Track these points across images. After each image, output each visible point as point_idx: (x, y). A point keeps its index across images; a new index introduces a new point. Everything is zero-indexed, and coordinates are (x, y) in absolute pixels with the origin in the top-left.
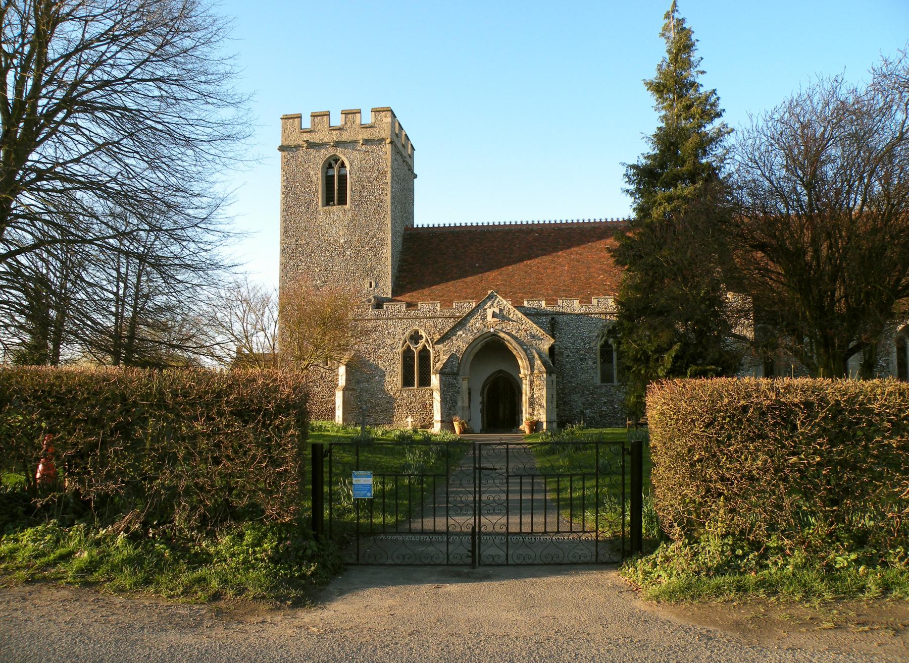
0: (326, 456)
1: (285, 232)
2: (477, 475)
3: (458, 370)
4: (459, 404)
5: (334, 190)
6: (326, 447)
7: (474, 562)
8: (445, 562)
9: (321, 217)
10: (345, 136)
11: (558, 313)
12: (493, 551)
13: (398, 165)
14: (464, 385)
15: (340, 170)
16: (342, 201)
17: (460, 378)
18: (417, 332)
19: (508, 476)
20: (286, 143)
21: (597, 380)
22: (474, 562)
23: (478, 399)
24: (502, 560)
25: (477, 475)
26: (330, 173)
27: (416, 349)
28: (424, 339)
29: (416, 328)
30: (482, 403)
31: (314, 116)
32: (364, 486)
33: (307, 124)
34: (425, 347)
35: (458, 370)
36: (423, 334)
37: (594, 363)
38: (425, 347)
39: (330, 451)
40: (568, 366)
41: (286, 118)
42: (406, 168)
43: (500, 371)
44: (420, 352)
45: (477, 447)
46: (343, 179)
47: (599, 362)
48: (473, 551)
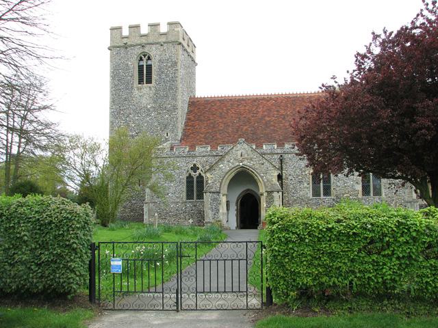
0: (96, 249)
1: (113, 102)
2: (179, 260)
3: (220, 190)
4: (221, 211)
5: (145, 75)
6: (97, 244)
7: (177, 308)
8: (245, 308)
9: (136, 92)
10: (151, 40)
11: (285, 153)
12: (189, 302)
13: (185, 58)
14: (224, 199)
15: (145, 63)
16: (149, 81)
17: (221, 195)
18: (195, 165)
19: (197, 260)
20: (113, 45)
21: (310, 195)
22: (177, 308)
23: (233, 208)
24: (194, 307)
25: (179, 260)
26: (141, 63)
27: (195, 175)
28: (200, 170)
29: (195, 162)
30: (237, 210)
31: (130, 27)
32: (117, 266)
33: (126, 32)
34: (200, 174)
35: (220, 190)
36: (200, 166)
37: (308, 184)
38: (200, 174)
39: (99, 247)
40: (291, 186)
41: (112, 29)
42: (190, 59)
43: (248, 190)
44: (197, 178)
45: (179, 244)
46: (149, 67)
47: (311, 184)
48: (177, 303)
